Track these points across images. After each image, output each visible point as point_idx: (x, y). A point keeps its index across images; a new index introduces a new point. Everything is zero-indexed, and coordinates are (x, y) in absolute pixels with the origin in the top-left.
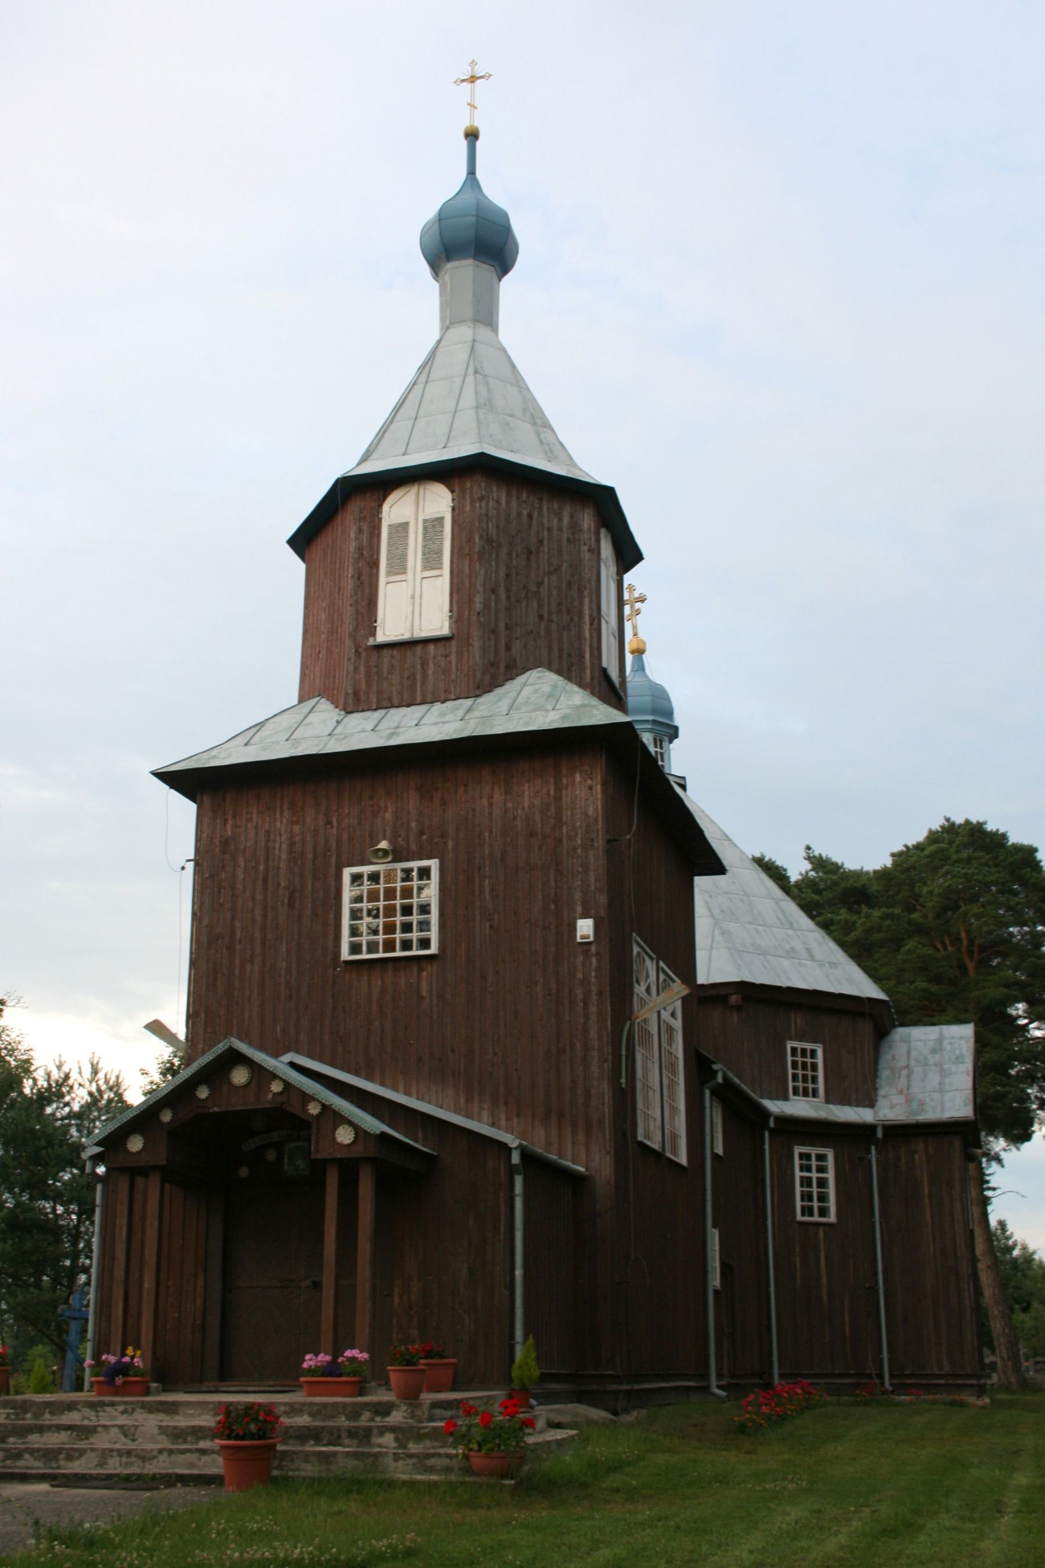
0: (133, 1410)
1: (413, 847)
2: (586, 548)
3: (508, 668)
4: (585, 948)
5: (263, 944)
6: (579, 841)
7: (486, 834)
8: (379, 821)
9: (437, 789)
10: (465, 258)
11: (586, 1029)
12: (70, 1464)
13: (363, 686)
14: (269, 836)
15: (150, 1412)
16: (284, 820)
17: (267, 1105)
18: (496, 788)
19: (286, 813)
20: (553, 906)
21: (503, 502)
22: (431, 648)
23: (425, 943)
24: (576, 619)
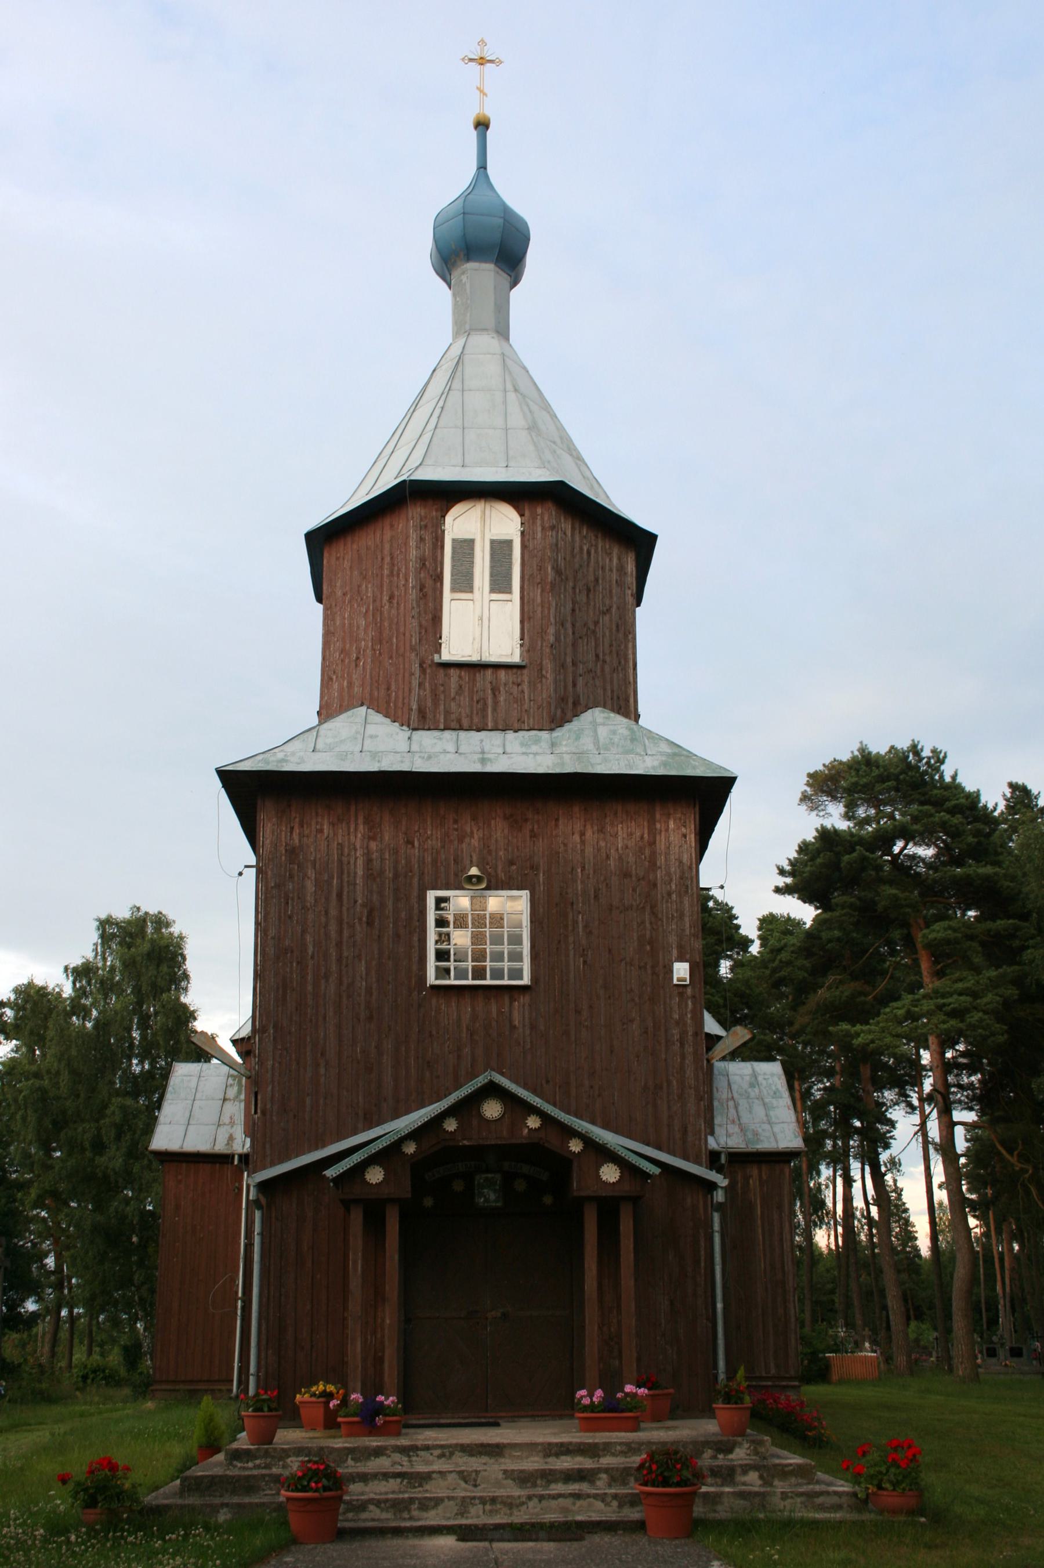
0: (452, 1454)
1: (502, 876)
2: (630, 592)
3: (576, 704)
4: (681, 990)
5: (339, 960)
6: (674, 887)
7: (579, 870)
8: (464, 846)
9: (526, 820)
10: (486, 262)
11: (682, 1069)
12: (425, 1514)
13: (429, 704)
14: (342, 849)
15: (471, 1455)
16: (359, 835)
17: (524, 1141)
18: (588, 826)
19: (361, 827)
20: (648, 948)
21: (569, 533)
22: (502, 674)
23: (517, 974)
24: (623, 662)
